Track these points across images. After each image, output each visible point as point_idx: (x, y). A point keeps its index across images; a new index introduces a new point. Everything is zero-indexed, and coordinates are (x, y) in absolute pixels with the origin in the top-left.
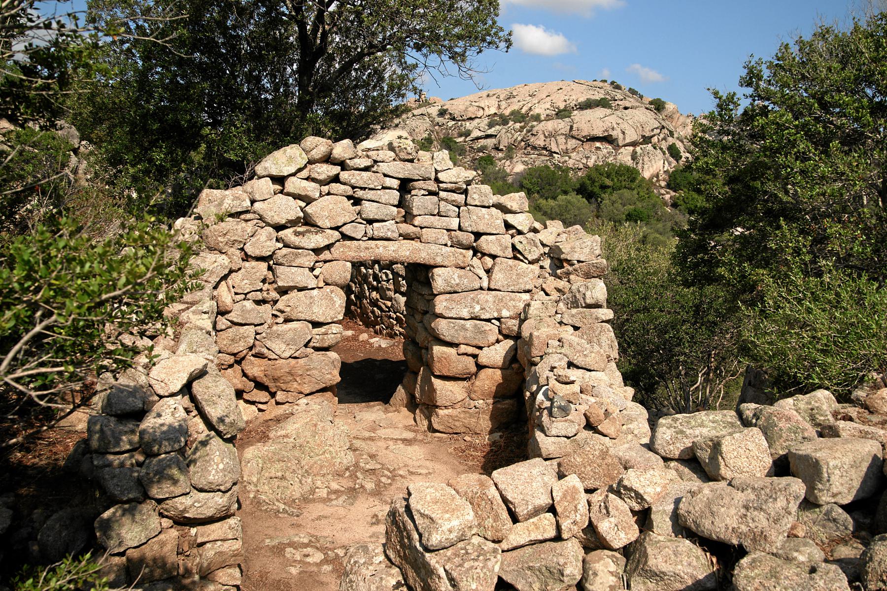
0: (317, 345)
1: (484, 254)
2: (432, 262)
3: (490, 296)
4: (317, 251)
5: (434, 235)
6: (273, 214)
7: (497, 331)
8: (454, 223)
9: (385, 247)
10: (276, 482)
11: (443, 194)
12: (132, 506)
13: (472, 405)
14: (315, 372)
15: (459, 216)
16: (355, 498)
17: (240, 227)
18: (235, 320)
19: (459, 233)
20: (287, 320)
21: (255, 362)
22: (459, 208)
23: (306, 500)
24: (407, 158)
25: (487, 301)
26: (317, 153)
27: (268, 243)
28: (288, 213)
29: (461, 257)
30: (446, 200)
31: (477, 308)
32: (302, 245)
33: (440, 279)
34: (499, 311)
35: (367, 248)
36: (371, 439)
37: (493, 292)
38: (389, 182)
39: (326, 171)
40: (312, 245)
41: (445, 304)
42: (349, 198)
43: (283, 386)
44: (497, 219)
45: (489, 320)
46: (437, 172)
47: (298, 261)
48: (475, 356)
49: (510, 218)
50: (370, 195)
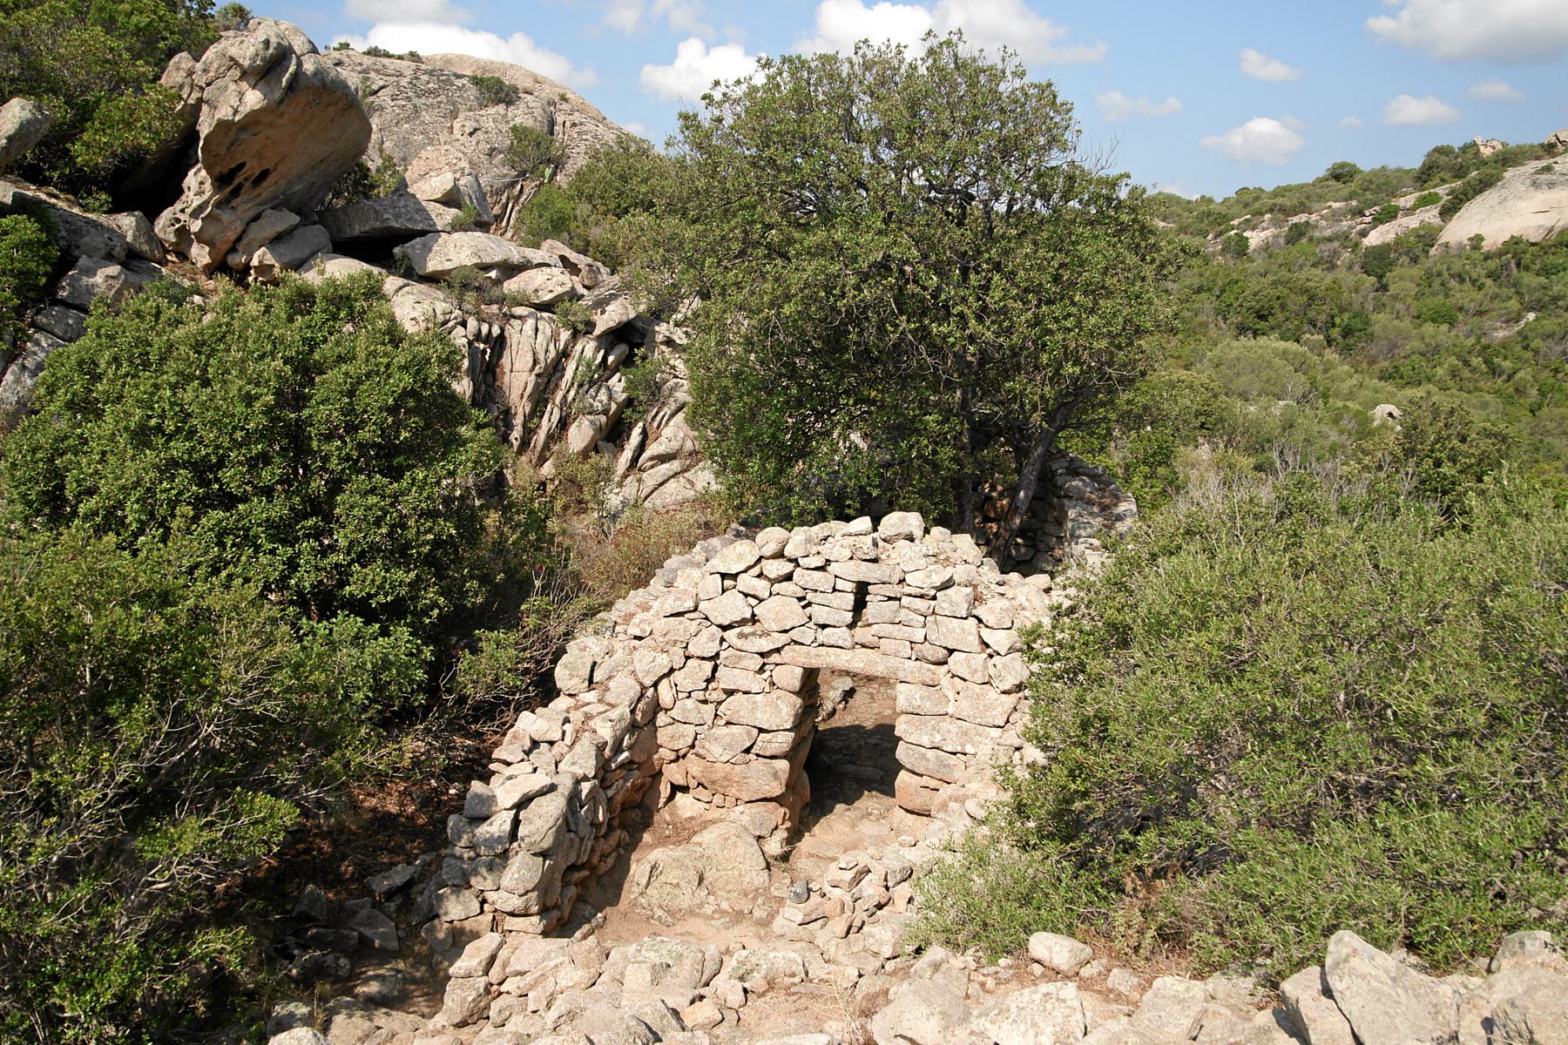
8: (919, 635)
10: (668, 888)
11: (905, 600)
12: (457, 889)
16: (738, 922)
20: (728, 723)
23: (692, 913)
34: (963, 745)
39: (776, 568)
47: (743, 664)
49: (987, 635)
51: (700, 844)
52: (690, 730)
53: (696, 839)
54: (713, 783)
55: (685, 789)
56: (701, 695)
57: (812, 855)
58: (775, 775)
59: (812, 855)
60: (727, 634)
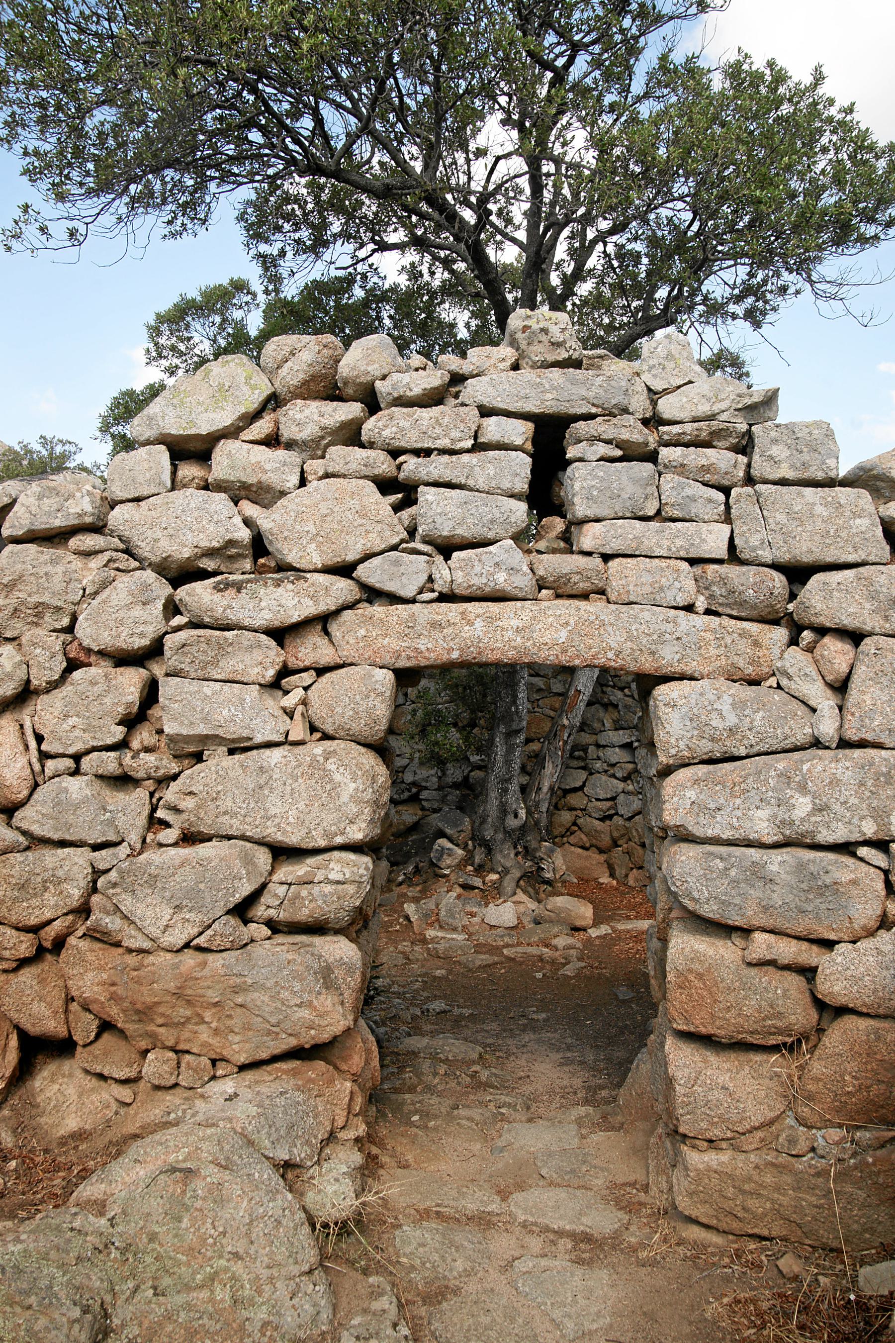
0: (282, 915)
1: (822, 631)
2: (647, 665)
3: (844, 766)
4: (280, 634)
5: (646, 578)
6: (159, 534)
7: (880, 886)
8: (714, 540)
9: (490, 620)
13: (802, 1146)
14: (258, 997)
15: (727, 519)
17: (59, 569)
18: (36, 829)
19: (732, 571)
20: (189, 838)
21: (90, 957)
22: (726, 491)
24: (551, 358)
25: (835, 782)
26: (293, 374)
27: (137, 612)
28: (203, 530)
29: (743, 645)
30: (681, 469)
31: (802, 806)
32: (233, 616)
33: (677, 716)
35: (436, 625)
36: (484, 1222)
37: (857, 753)
38: (494, 428)
39: (308, 417)
40: (265, 617)
41: (691, 794)
42: (385, 485)
43: (168, 1036)
44: (855, 515)
45: (846, 848)
46: (654, 395)
47: (228, 666)
48: (809, 972)
50: (437, 467)
51: (100, 1207)
52: (78, 861)
53: (89, 1190)
54: (144, 1013)
55: (63, 1047)
56: (109, 762)
57: (424, 1215)
58: (326, 976)
59: (424, 1215)
60: (186, 593)
